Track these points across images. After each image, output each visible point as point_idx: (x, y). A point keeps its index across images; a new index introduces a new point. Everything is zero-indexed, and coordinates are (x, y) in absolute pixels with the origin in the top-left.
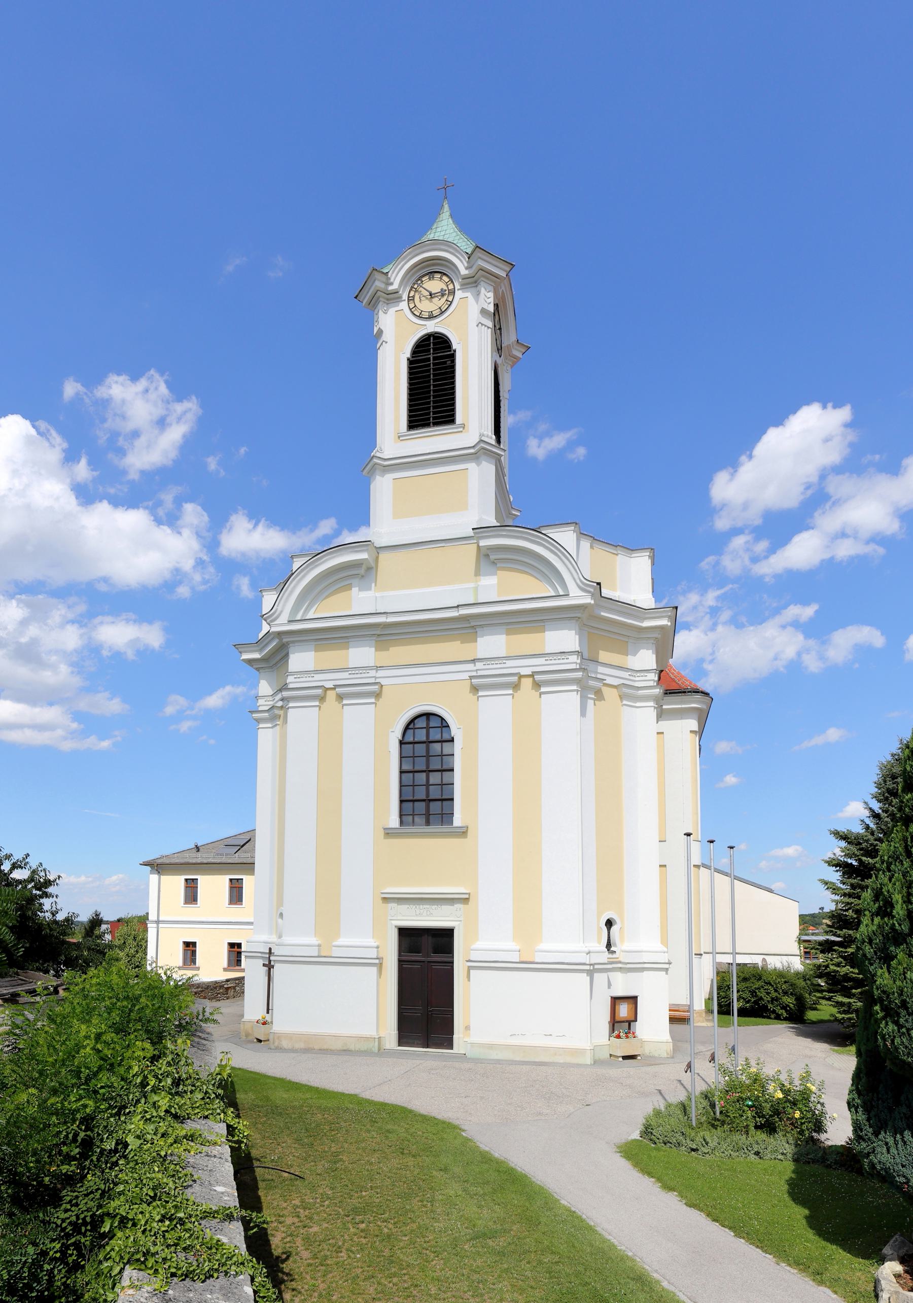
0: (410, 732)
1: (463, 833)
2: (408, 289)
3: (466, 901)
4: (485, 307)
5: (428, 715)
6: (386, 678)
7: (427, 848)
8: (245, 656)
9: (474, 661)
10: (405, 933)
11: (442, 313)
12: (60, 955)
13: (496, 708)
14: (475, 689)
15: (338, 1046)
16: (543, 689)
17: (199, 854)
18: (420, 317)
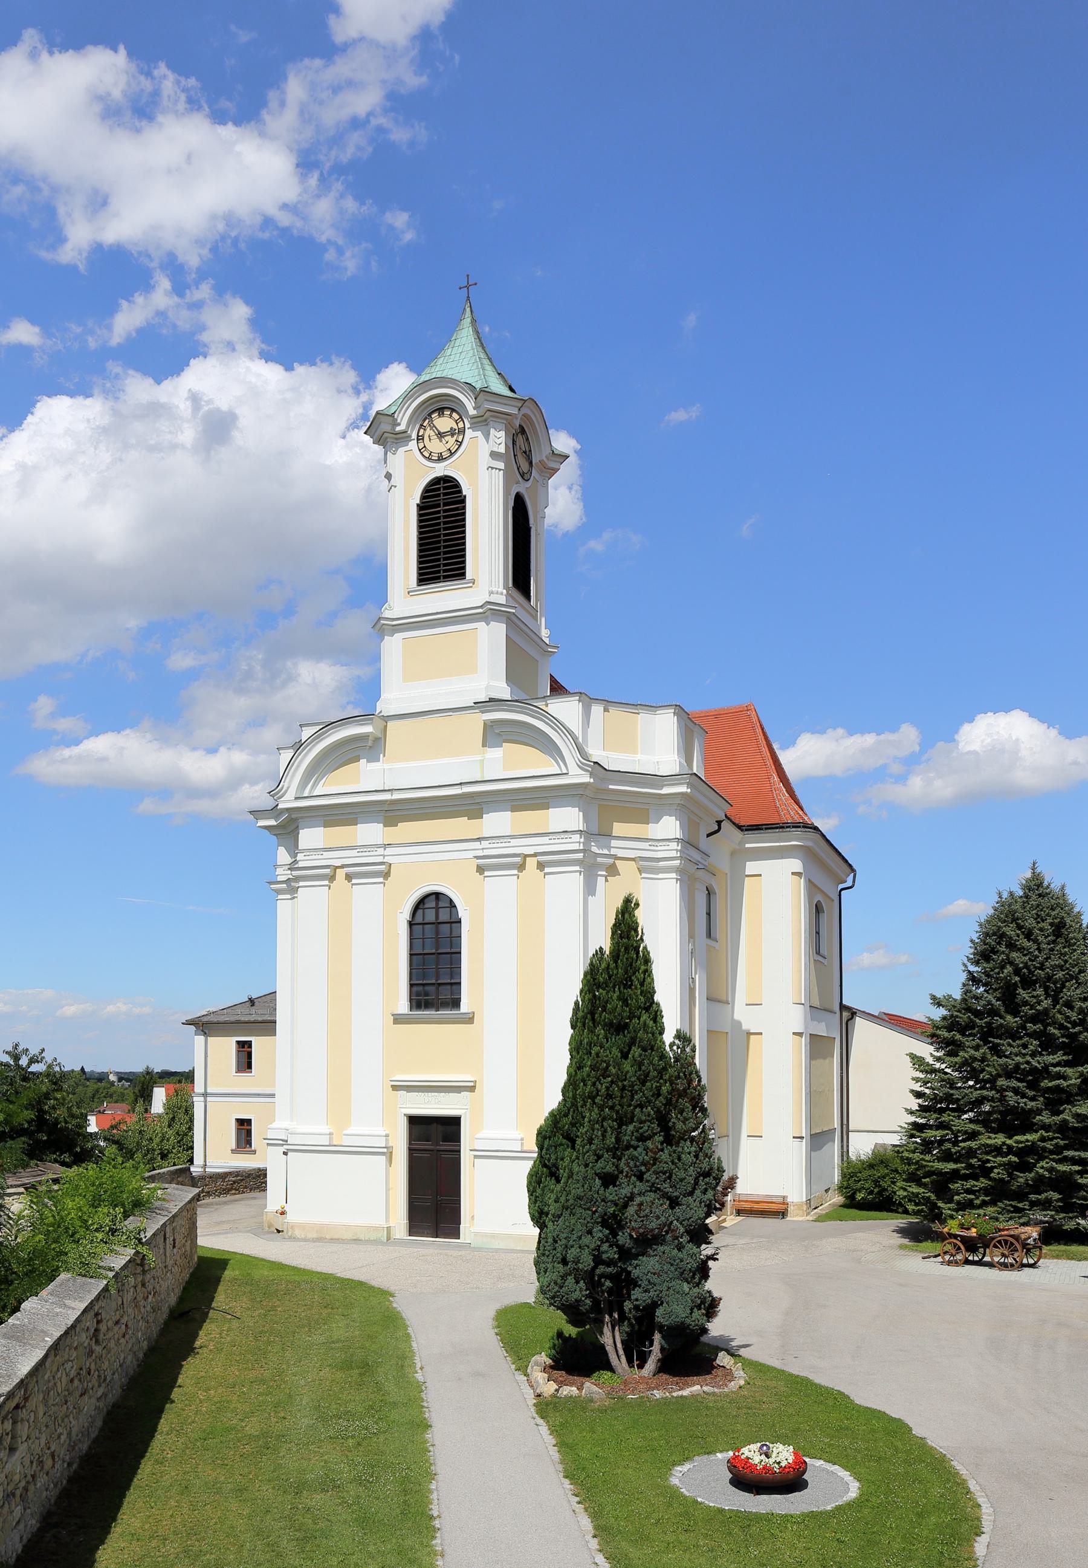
0: (420, 912)
1: (469, 1019)
2: (418, 426)
3: (472, 1089)
4: (495, 449)
5: (437, 895)
6: (392, 856)
7: (434, 1034)
8: (261, 823)
9: (479, 839)
10: (416, 1122)
11: (452, 454)
12: (76, 1146)
13: (502, 887)
14: (481, 869)
15: (348, 1236)
16: (547, 870)
17: (253, 1010)
18: (429, 459)
